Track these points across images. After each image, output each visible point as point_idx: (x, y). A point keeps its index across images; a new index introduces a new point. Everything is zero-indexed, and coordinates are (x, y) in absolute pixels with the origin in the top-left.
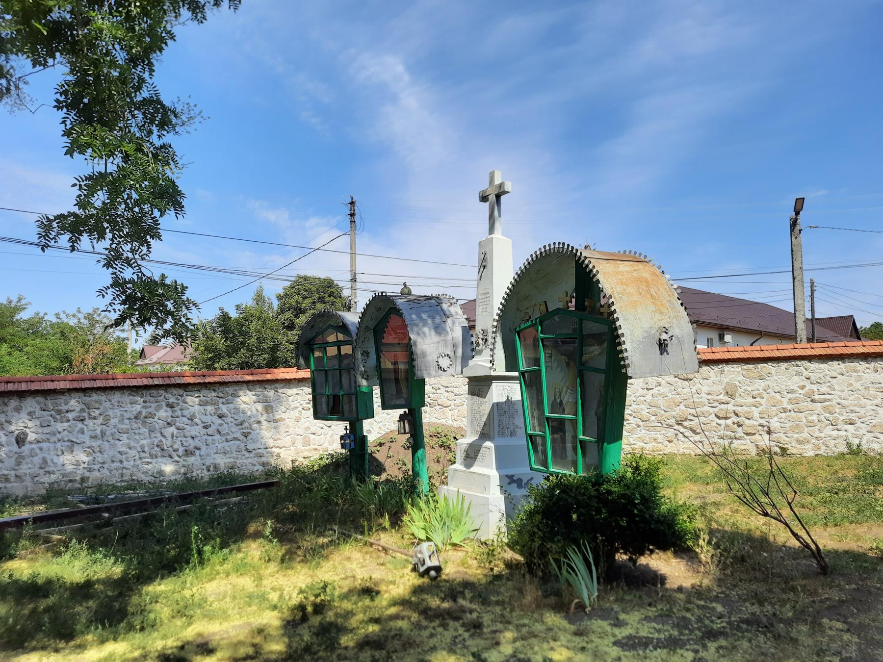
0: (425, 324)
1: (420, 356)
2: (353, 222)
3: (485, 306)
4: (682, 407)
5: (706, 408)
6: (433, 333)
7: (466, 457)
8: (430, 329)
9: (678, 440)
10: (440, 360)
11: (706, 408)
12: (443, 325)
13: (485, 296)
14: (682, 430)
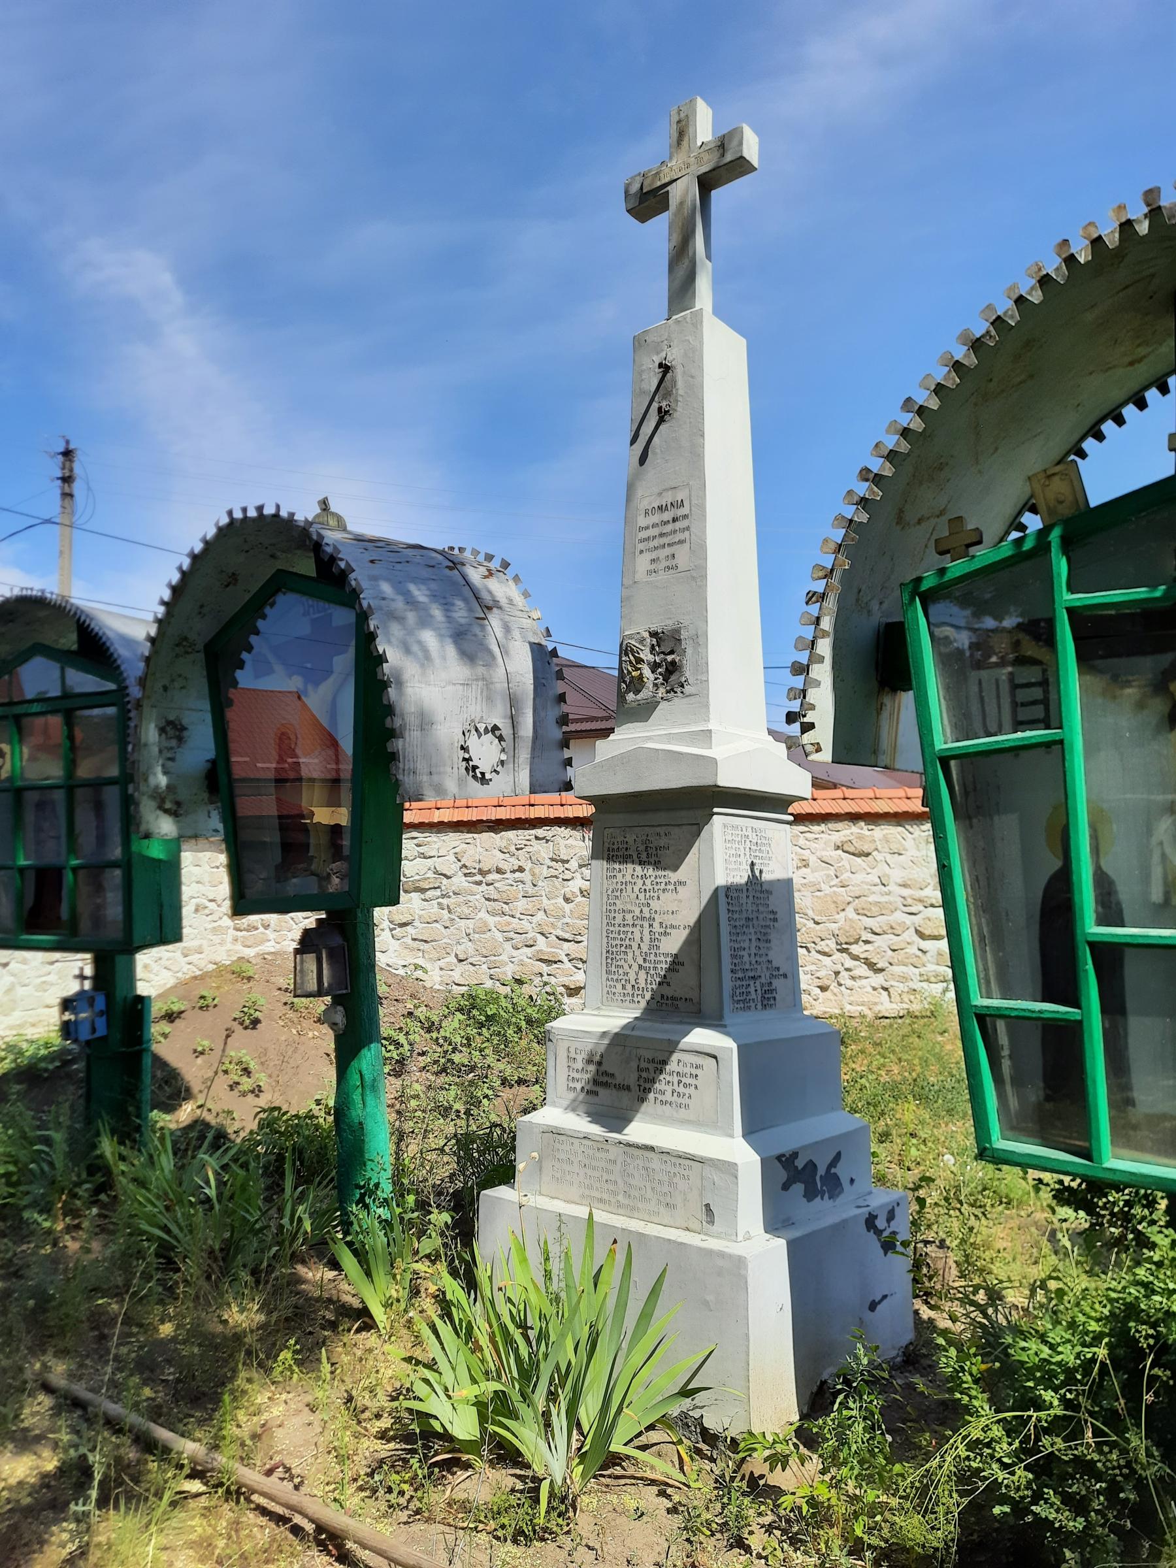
0: (425, 621)
1: (412, 720)
2: (67, 495)
3: (668, 551)
4: (850, 912)
5: (899, 916)
6: (451, 651)
7: (595, 1082)
8: (441, 637)
9: (840, 985)
10: (473, 741)
11: (899, 916)
12: (477, 630)
13: (667, 516)
14: (849, 963)
